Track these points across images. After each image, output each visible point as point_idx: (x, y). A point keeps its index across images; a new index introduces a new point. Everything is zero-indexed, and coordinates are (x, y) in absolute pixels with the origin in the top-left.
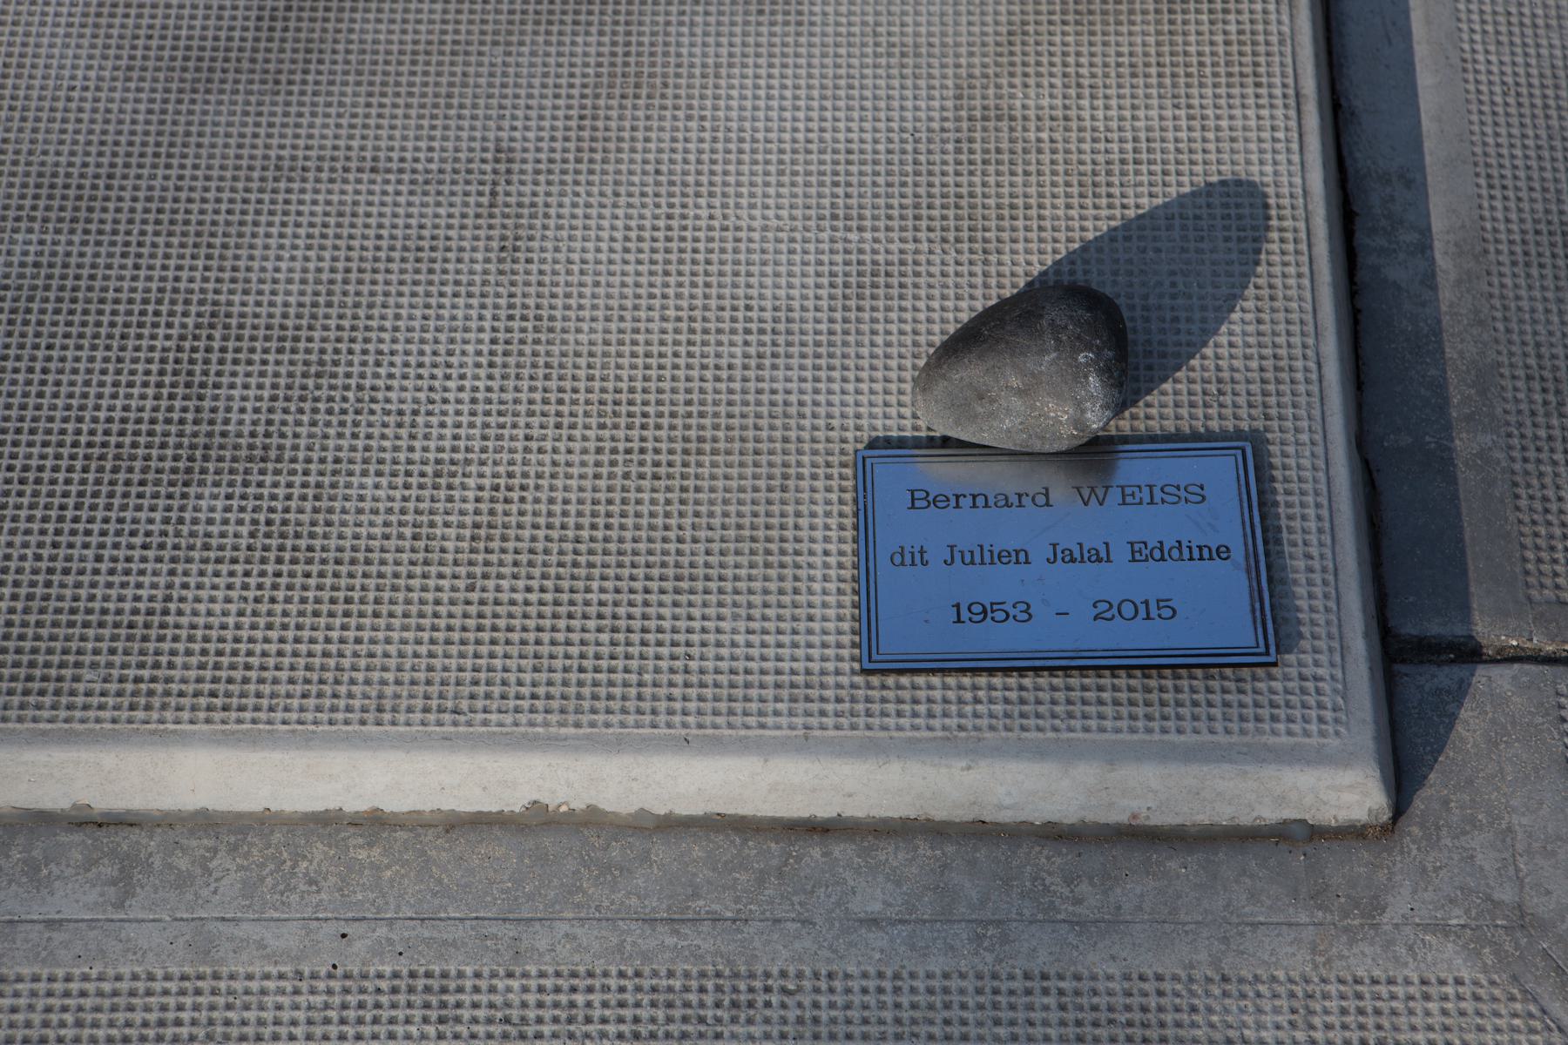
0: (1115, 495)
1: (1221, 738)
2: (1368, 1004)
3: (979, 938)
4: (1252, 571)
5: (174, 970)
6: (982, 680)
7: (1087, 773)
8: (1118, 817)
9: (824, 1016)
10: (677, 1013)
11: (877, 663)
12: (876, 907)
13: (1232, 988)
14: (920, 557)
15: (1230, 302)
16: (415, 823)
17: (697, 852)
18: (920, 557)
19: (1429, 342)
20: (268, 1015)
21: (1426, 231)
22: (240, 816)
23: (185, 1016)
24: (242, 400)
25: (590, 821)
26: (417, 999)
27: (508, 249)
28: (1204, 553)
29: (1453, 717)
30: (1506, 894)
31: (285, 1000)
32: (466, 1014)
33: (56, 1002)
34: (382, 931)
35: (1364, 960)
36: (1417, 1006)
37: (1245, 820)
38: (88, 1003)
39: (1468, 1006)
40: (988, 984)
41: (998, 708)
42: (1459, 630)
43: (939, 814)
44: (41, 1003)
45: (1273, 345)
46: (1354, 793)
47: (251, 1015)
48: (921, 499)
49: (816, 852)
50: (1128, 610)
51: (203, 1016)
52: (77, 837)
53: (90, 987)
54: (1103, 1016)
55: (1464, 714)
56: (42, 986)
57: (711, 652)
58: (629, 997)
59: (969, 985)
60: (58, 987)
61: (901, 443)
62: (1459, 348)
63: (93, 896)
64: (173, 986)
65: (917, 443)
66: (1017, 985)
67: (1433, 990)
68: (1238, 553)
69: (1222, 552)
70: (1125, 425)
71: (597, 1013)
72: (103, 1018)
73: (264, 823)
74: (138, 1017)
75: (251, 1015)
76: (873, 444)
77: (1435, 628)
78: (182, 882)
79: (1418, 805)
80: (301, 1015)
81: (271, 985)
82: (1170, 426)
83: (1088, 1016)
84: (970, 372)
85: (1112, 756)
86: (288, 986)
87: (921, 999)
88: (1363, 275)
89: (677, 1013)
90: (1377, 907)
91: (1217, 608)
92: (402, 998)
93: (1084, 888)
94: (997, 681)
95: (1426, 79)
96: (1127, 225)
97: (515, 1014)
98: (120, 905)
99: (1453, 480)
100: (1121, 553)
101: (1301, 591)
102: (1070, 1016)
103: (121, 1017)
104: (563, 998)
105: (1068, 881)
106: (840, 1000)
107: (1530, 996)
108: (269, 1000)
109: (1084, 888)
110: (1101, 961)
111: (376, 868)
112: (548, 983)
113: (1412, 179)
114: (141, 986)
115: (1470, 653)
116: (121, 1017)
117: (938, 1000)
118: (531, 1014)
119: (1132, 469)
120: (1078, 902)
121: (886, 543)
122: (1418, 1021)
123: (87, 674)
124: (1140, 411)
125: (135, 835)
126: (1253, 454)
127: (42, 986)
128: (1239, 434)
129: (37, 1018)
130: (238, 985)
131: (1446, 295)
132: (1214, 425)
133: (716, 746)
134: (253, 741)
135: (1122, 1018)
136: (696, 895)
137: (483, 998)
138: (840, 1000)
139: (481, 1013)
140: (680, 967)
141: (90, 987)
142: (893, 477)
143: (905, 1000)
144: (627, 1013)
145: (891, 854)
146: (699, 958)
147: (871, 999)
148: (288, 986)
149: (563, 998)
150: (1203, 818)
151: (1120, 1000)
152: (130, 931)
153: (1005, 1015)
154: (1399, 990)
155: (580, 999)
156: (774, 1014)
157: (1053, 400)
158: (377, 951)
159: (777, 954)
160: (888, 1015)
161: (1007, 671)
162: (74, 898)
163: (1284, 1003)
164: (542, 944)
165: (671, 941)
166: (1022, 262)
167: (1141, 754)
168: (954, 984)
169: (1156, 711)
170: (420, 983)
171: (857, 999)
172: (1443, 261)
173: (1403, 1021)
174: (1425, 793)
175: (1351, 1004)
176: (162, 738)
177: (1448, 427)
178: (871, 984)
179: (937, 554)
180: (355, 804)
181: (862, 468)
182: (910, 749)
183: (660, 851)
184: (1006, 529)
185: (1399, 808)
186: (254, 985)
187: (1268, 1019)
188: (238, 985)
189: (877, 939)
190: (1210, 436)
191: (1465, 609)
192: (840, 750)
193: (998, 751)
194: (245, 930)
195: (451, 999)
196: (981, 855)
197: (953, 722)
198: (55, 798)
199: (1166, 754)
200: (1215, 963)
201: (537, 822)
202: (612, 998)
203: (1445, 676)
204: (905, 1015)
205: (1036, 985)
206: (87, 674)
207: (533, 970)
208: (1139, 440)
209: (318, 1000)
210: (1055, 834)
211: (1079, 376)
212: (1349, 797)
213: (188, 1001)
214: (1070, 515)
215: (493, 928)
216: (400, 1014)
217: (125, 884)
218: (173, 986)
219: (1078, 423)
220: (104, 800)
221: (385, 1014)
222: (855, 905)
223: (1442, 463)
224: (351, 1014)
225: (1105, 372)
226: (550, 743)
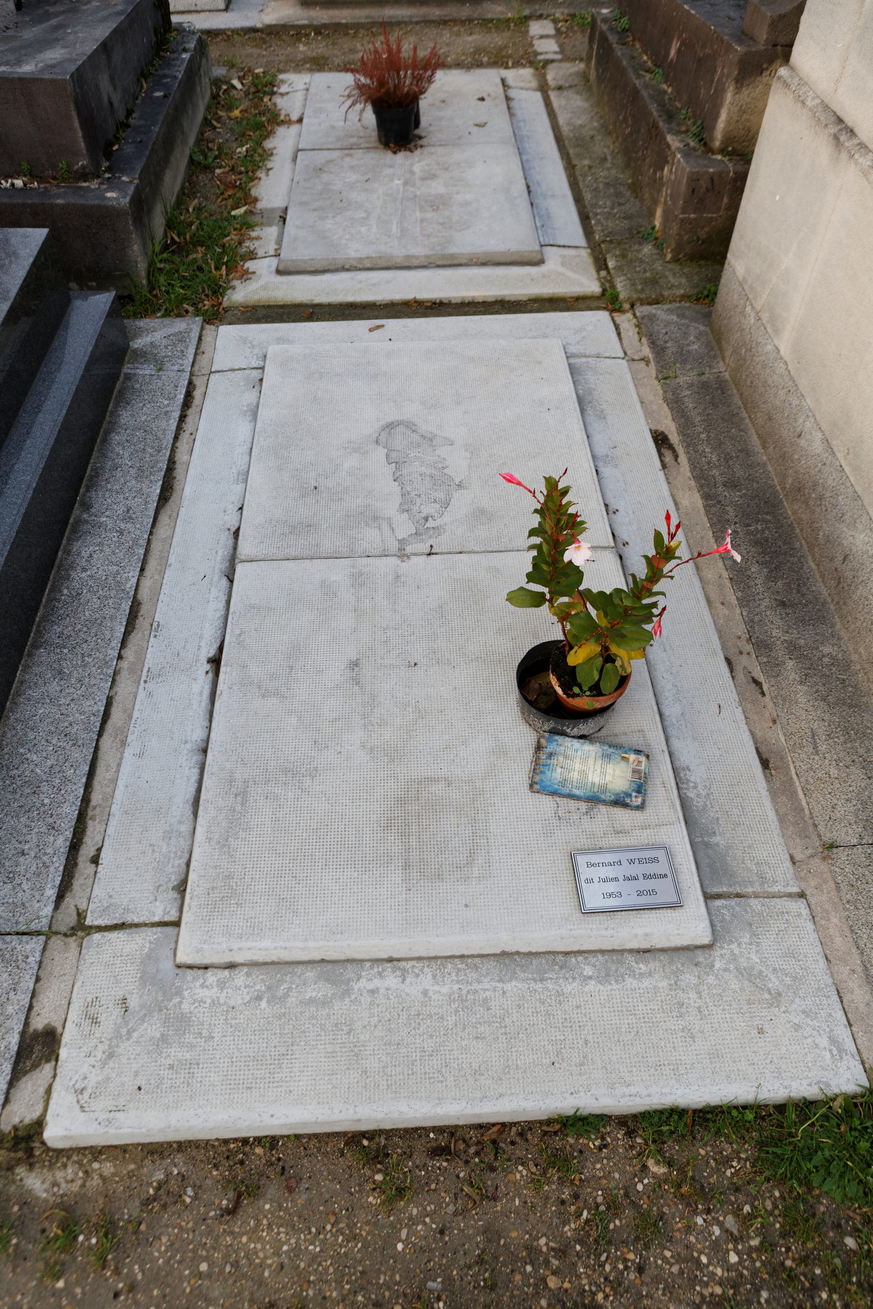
14: (592, 881)
50: (645, 893)
52: (389, 965)
90: (712, 966)
100: (641, 877)
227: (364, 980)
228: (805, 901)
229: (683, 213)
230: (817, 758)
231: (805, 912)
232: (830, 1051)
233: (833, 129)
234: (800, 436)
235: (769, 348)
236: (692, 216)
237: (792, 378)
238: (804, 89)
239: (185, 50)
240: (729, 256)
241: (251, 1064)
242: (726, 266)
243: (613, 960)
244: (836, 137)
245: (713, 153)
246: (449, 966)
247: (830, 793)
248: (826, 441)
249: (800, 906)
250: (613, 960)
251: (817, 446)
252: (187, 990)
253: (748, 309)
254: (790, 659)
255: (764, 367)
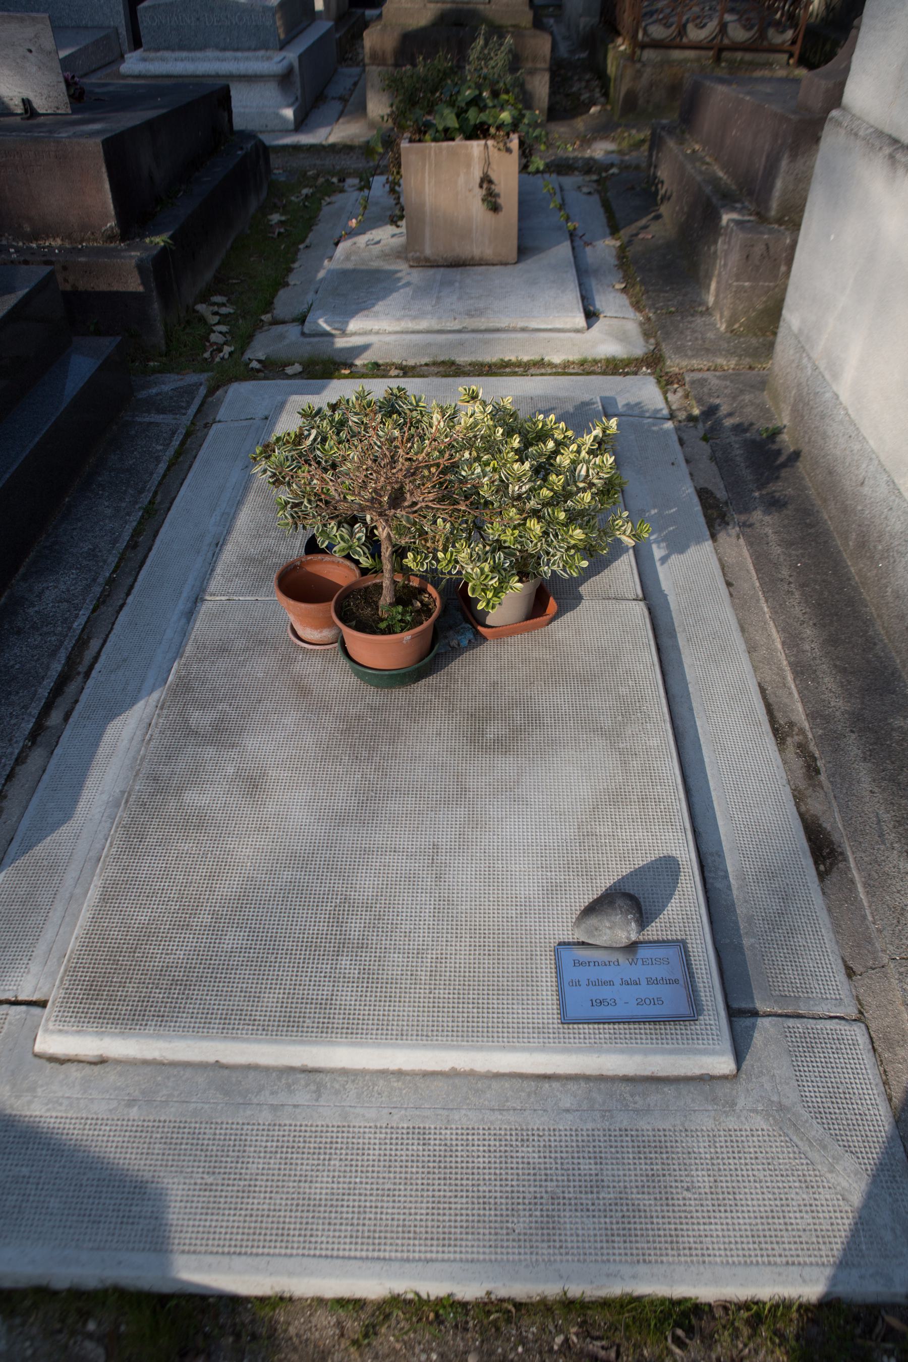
0: (640, 962)
1: (681, 1046)
2: (734, 1138)
3: (603, 1116)
4: (687, 988)
5: (335, 1124)
6: (601, 1026)
7: (638, 1058)
8: (647, 1073)
9: (553, 1144)
10: (503, 1143)
11: (566, 1020)
12: (568, 1105)
13: (689, 1133)
14: (578, 984)
15: (671, 896)
16: (413, 1074)
17: (507, 1085)
18: (578, 984)
19: (731, 908)
20: (366, 1141)
21: (726, 871)
22: (355, 1070)
23: (339, 1140)
24: (355, 927)
25: (471, 1074)
26: (416, 1136)
27: (438, 877)
28: (670, 982)
29: (752, 1036)
30: (775, 1098)
31: (372, 1136)
32: (432, 1142)
33: (297, 1134)
34: (403, 1112)
35: (731, 1123)
36: (750, 1139)
37: (689, 1074)
38: (308, 1134)
39: (766, 1138)
40: (607, 1133)
41: (607, 1036)
42: (751, 1006)
43: (588, 1072)
44: (292, 1134)
45: (684, 911)
46: (724, 1064)
47: (361, 1141)
48: (578, 963)
49: (547, 1085)
50: (648, 1001)
51: (345, 1140)
52: (303, 1076)
53: (308, 1129)
54: (647, 1144)
55: (755, 1035)
56: (293, 1128)
57: (510, 1016)
58: (487, 1137)
59: (601, 1133)
60: (298, 1128)
61: (569, 944)
62: (741, 910)
63: (308, 1097)
64: (335, 1129)
65: (574, 944)
66: (617, 1133)
67: (755, 1133)
68: (682, 982)
69: (676, 981)
70: (641, 937)
71: (476, 1143)
72: (313, 1140)
73: (363, 1073)
74: (324, 1140)
75: (361, 1141)
76: (560, 944)
77: (744, 1005)
78: (337, 1092)
79: (744, 1067)
80: (377, 1141)
81: (367, 1130)
82: (655, 938)
83: (642, 1144)
84: (593, 921)
85: (646, 1052)
86: (373, 1130)
87: (585, 1138)
88: (708, 886)
89: (503, 1143)
90: (733, 1104)
91: (673, 1000)
92: (410, 1136)
93: (637, 1098)
94: (606, 1026)
95: (720, 823)
96: (636, 870)
97: (448, 1143)
98: (317, 1100)
99: (744, 955)
100: (643, 982)
101: (702, 994)
102: (636, 1144)
103: (318, 1140)
104: (465, 1137)
105: (632, 1096)
106: (558, 1138)
107: (786, 1135)
108: (367, 1136)
109: (637, 1098)
110: (643, 1124)
111: (400, 1089)
112: (459, 1132)
113: (720, 854)
114: (324, 1129)
115: (755, 1014)
116: (318, 1140)
117: (591, 1139)
118: (454, 1143)
119: (643, 953)
120: (635, 1103)
121: (567, 978)
122: (750, 1144)
123: (307, 1020)
124: (645, 932)
125: (321, 1075)
126: (682, 945)
127: (293, 1128)
128: (677, 941)
129: (291, 1139)
130: (356, 1130)
131: (735, 892)
132: (670, 937)
133: (514, 1049)
134: (361, 1045)
135: (653, 1145)
136: (507, 1101)
137: (438, 1137)
138: (558, 1138)
139: (437, 1142)
140: (503, 1127)
141: (308, 1129)
142: (568, 955)
143: (580, 1139)
144: (486, 1143)
145: (572, 1086)
146: (509, 1123)
147: (568, 1138)
148: (373, 1130)
149: (465, 1137)
150: (676, 1073)
151: (652, 1138)
152: (321, 1110)
153: (614, 1144)
154: (744, 1133)
155: (470, 1137)
156: (536, 1144)
157: (618, 930)
158: (401, 1119)
159: (536, 1122)
160: (574, 1144)
161: (609, 1023)
162: (302, 1097)
163: (706, 1138)
164: (457, 1118)
165: (500, 1117)
166: (603, 883)
167: (655, 1052)
168: (596, 1133)
169: (659, 1036)
170: (417, 1131)
171: (563, 1138)
172: (733, 882)
173: (746, 1144)
174: (745, 1063)
175: (728, 1139)
176: (332, 1043)
177: (740, 936)
178: (568, 1133)
179: (584, 983)
180: (393, 1067)
181: (556, 952)
182: (579, 1050)
183: (495, 1085)
184: (606, 974)
185: (739, 1069)
186: (362, 1130)
187: (701, 1144)
188: (356, 1130)
189: (569, 1116)
190: (668, 941)
191: (752, 998)
192: (555, 1050)
193: (608, 1051)
194: (358, 1110)
195: (427, 1137)
196: (602, 1086)
197: (592, 1041)
198: (296, 1062)
199: (663, 1052)
200: (683, 1124)
201: (453, 1074)
202: (481, 1137)
203: (748, 1021)
204: (580, 1144)
205: (623, 1133)
206: (307, 1020)
207: (454, 1127)
208: (646, 942)
209: (383, 1136)
210: (626, 1079)
211: (629, 923)
212: (723, 1066)
213: (340, 1135)
214: (625, 968)
215: (440, 1112)
216: (410, 1142)
217: (318, 1093)
218: (335, 1129)
219: (628, 938)
220: (311, 1063)
221: (405, 1142)
222: (561, 1105)
223: (739, 948)
224: (394, 1141)
225: (637, 921)
226: (458, 1048)
227: (267, 1093)
228: (863, 1025)
229: (737, 280)
230: (882, 847)
231: (862, 1040)
232: (893, 1230)
233: (887, 150)
234: (862, 483)
235: (828, 395)
236: (747, 284)
237: (852, 422)
238: (857, 123)
239: (242, 149)
240: (784, 312)
241: (104, 1189)
242: (781, 323)
243: (599, 1089)
244: (891, 157)
245: (770, 223)
246: (381, 1082)
247: (899, 892)
248: (891, 483)
249: (858, 1033)
250: (599, 1089)
251: (883, 489)
252: (42, 1086)
253: (805, 361)
254: (852, 731)
255: (823, 417)
